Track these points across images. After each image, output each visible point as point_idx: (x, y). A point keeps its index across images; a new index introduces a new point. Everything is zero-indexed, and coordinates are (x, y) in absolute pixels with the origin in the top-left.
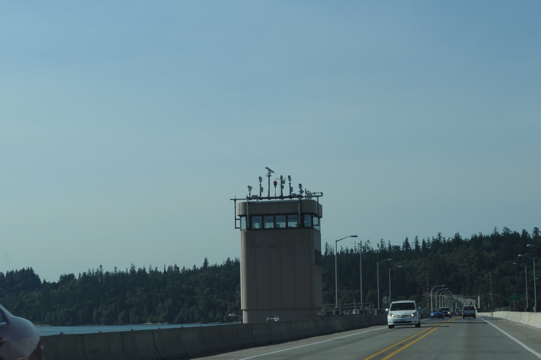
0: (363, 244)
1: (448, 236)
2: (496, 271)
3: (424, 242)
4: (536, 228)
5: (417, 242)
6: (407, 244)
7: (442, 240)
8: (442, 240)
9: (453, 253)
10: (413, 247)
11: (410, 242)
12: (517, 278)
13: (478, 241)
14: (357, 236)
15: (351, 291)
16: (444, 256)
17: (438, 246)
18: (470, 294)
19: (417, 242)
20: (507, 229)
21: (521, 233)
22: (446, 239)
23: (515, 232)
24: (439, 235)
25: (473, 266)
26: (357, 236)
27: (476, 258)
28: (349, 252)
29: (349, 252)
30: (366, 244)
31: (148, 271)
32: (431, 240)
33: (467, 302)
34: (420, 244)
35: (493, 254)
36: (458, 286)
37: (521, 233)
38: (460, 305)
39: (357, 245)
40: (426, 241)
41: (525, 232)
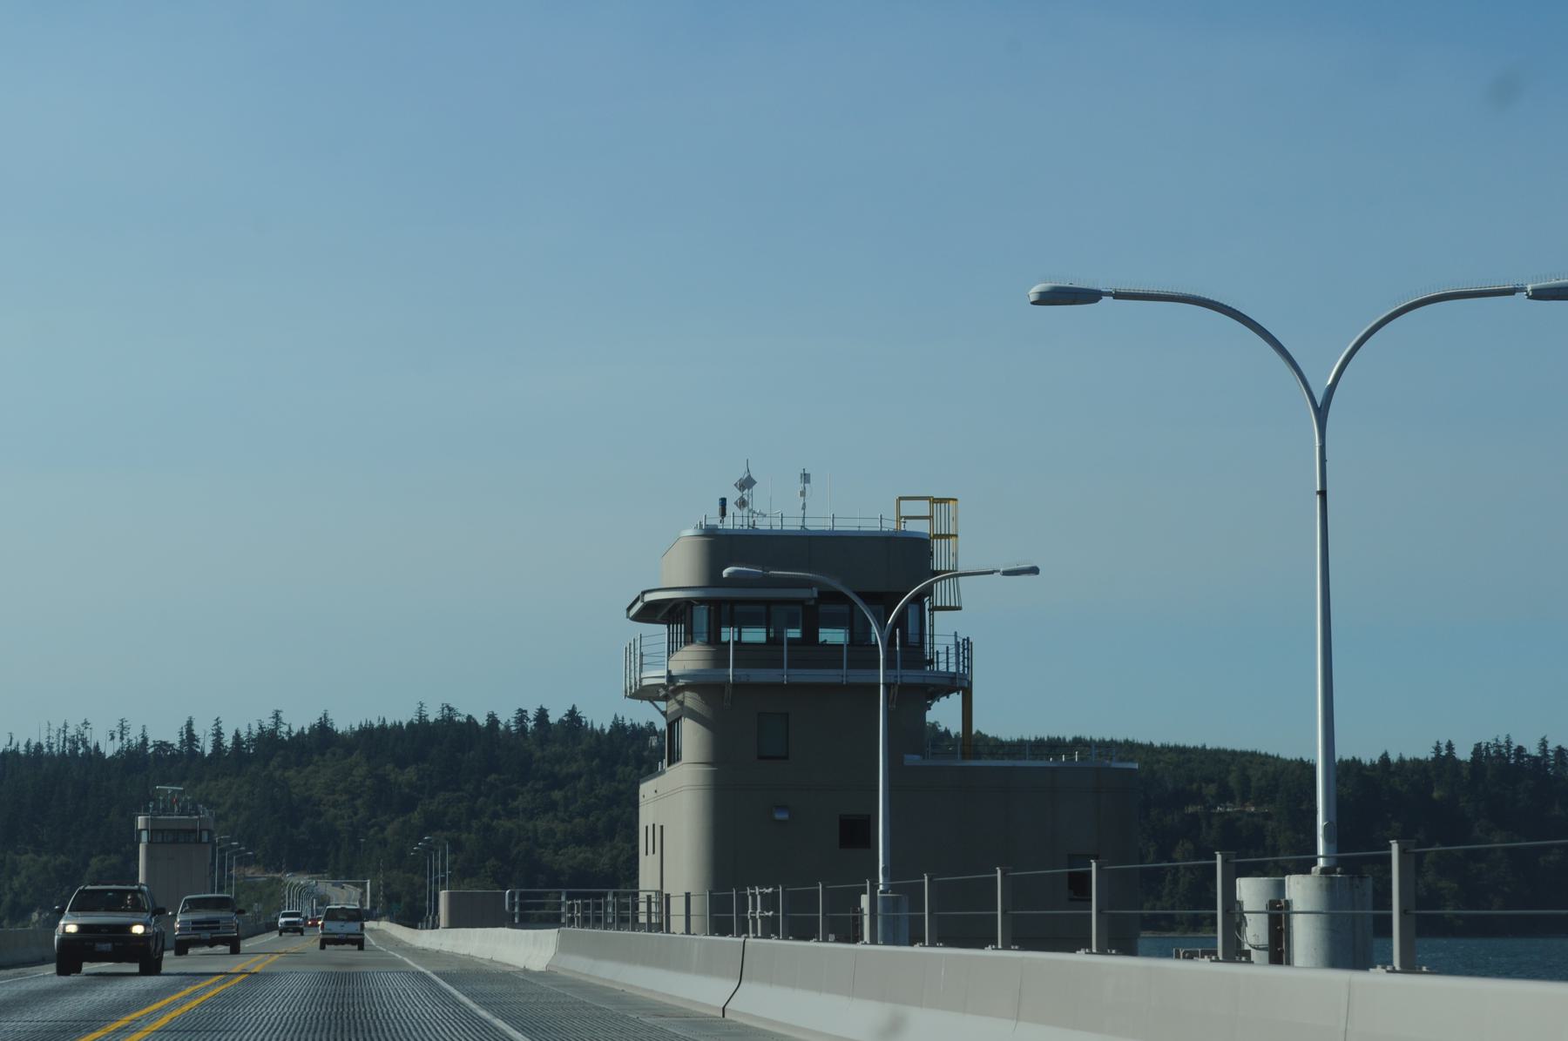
0: (71, 732)
1: (299, 721)
2: (416, 817)
3: (237, 735)
4: (521, 711)
5: (218, 734)
6: (190, 737)
7: (284, 729)
8: (284, 729)
9: (311, 768)
10: (22, 750)
11: (197, 731)
12: (464, 836)
13: (374, 739)
14: (1034, 571)
15: (45, 858)
16: (291, 773)
17: (270, 747)
18: (347, 873)
19: (218, 734)
20: (450, 709)
21: (482, 721)
22: (295, 730)
23: (469, 717)
24: (277, 716)
25: (359, 802)
26: (1034, 571)
27: (368, 782)
28: (530, 725)
29: (530, 725)
30: (79, 732)
31: (22, 750)
32: (255, 730)
33: (345, 896)
34: (228, 741)
35: (410, 774)
36: (318, 855)
37: (482, 721)
38: (323, 901)
39: (53, 734)
40: (244, 736)
41: (493, 720)
